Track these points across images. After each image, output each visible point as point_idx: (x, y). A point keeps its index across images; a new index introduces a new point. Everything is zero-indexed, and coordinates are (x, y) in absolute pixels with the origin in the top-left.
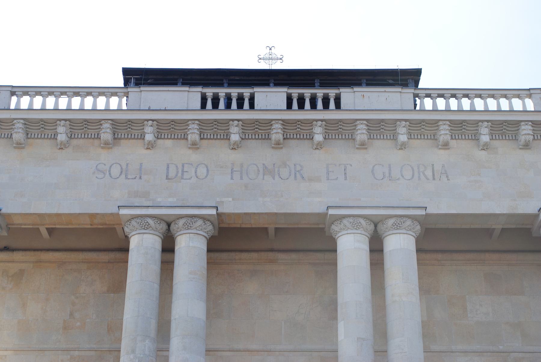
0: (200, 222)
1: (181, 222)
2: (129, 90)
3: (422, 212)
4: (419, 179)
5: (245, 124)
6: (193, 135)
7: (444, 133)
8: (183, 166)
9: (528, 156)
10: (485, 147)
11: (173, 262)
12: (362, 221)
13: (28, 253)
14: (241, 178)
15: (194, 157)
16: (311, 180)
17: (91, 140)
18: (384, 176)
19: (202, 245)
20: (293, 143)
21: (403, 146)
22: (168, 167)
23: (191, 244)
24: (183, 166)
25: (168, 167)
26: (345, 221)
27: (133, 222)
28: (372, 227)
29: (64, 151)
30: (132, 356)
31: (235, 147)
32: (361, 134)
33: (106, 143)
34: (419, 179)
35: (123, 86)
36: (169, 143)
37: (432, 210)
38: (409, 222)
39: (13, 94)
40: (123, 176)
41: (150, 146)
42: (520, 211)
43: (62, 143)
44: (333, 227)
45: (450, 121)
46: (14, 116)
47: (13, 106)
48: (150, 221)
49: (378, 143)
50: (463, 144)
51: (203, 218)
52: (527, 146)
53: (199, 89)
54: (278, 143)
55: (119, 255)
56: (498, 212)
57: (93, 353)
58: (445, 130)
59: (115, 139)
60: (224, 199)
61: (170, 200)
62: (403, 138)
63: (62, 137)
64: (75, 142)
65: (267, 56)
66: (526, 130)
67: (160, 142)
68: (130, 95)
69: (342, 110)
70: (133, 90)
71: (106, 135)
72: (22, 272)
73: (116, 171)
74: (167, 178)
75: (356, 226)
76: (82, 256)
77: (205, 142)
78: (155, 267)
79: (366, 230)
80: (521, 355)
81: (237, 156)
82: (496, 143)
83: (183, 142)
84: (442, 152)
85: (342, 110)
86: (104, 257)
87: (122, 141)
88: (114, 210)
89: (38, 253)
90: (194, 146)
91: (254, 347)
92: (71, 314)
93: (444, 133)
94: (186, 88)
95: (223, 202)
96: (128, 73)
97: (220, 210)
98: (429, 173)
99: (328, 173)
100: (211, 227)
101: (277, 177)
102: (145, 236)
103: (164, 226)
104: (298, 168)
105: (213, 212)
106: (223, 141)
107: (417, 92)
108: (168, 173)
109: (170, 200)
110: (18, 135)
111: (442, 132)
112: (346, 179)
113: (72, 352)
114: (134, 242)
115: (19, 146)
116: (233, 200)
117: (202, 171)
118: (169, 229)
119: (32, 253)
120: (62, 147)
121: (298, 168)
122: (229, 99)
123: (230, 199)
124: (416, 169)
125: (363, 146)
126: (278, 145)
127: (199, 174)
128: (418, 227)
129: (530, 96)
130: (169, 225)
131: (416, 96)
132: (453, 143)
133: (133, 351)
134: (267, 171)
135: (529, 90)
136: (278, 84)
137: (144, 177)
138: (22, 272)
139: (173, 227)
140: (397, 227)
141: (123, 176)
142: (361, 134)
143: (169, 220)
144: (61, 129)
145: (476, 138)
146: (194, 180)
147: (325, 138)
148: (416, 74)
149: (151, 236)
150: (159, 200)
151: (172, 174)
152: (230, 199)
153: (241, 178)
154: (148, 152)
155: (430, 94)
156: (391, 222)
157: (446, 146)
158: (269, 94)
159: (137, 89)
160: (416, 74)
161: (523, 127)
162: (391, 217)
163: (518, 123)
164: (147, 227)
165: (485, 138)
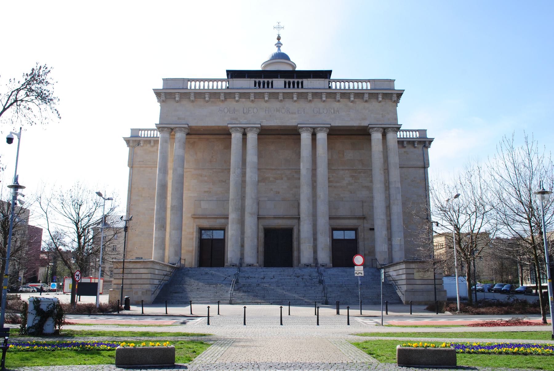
0: (255, 129)
1: (249, 129)
2: (229, 80)
3: (329, 126)
4: (329, 113)
5: (270, 93)
6: (252, 98)
7: (338, 96)
8: (249, 108)
9: (367, 105)
10: (352, 102)
11: (246, 139)
12: (309, 129)
13: (196, 135)
14: (269, 113)
15: (252, 105)
16: (292, 113)
17: (217, 99)
18: (317, 112)
19: (255, 136)
20: (286, 100)
21: (324, 101)
22: (244, 109)
23: (252, 137)
24: (249, 108)
25: (244, 109)
26: (304, 129)
27: (233, 129)
28: (313, 130)
29: (208, 103)
30: (234, 174)
31: (266, 102)
32: (310, 97)
33: (222, 101)
34: (329, 113)
35: (226, 78)
36: (244, 100)
37: (333, 124)
38: (325, 129)
39: (189, 81)
40: (228, 112)
41: (237, 101)
42: (362, 125)
43: (207, 100)
44: (300, 130)
45: (340, 93)
46: (190, 91)
47: (334, 87)
48: (238, 129)
49: (315, 100)
50: (345, 100)
51: (256, 127)
52: (366, 101)
53: (254, 79)
54: (281, 100)
55: (227, 136)
56: (355, 125)
57: (219, 170)
58: (338, 96)
59: (225, 98)
60: (263, 121)
61: (245, 121)
62: (324, 99)
63: (207, 99)
64: (211, 100)
65: (277, 26)
66: (366, 96)
67: (241, 99)
68: (230, 81)
69: (305, 89)
70: (230, 80)
71: (222, 98)
72: (194, 142)
73: (226, 110)
74: (244, 113)
75: (307, 130)
76: (215, 136)
77: (256, 99)
78: (240, 144)
79: (310, 131)
80: (361, 170)
81: (266, 105)
82: (356, 100)
83: (248, 99)
84: (337, 103)
85: (305, 89)
86: (222, 137)
87: (228, 99)
88: (226, 125)
89: (200, 136)
90: (252, 101)
91: (273, 168)
92: (212, 157)
93: (338, 96)
94: (249, 79)
95: (262, 122)
96: (229, 72)
97: (262, 125)
98: (333, 111)
99: (298, 111)
100: (259, 130)
101: (281, 113)
102: (237, 134)
103: (243, 130)
104: (288, 109)
105: (259, 126)
106: (262, 99)
107: (330, 80)
108: (244, 111)
109: (245, 121)
110: (192, 98)
111: (338, 97)
112: (304, 113)
113: (213, 170)
114: (233, 135)
115: (193, 101)
116: (266, 121)
117: (255, 110)
118: (244, 131)
119: (198, 136)
120: (207, 102)
121: (288, 109)
122: (294, 83)
123: (265, 121)
124: (328, 109)
125: (310, 101)
126: (281, 101)
127: (254, 111)
128: (328, 130)
129: (369, 82)
130: (245, 129)
131: (329, 82)
132: (341, 100)
133: (235, 173)
134: (278, 110)
135: (369, 80)
136: (282, 77)
137: (236, 113)
138: (194, 142)
139: (246, 130)
140: (321, 130)
141: (228, 112)
142: (310, 97)
143: (245, 128)
144: (207, 96)
145: (349, 98)
146: (253, 114)
147: (297, 98)
148: (330, 72)
149: (239, 134)
150: (241, 121)
151: (245, 112)
152: (265, 121)
153: (269, 113)
154: (237, 103)
155: (336, 81)
156: (319, 129)
157: (339, 101)
158: (278, 81)
159: (232, 80)
160: (330, 72)
161: (365, 95)
162: (319, 127)
163: (364, 93)
164: (237, 131)
165: (352, 99)
